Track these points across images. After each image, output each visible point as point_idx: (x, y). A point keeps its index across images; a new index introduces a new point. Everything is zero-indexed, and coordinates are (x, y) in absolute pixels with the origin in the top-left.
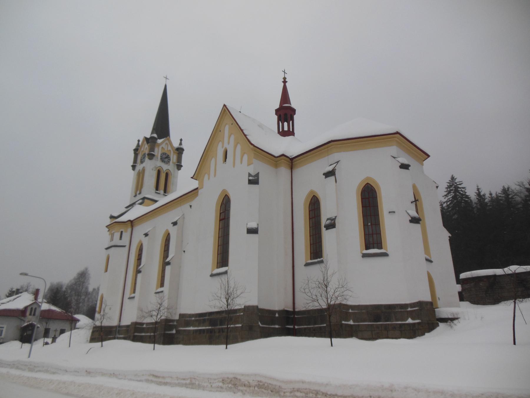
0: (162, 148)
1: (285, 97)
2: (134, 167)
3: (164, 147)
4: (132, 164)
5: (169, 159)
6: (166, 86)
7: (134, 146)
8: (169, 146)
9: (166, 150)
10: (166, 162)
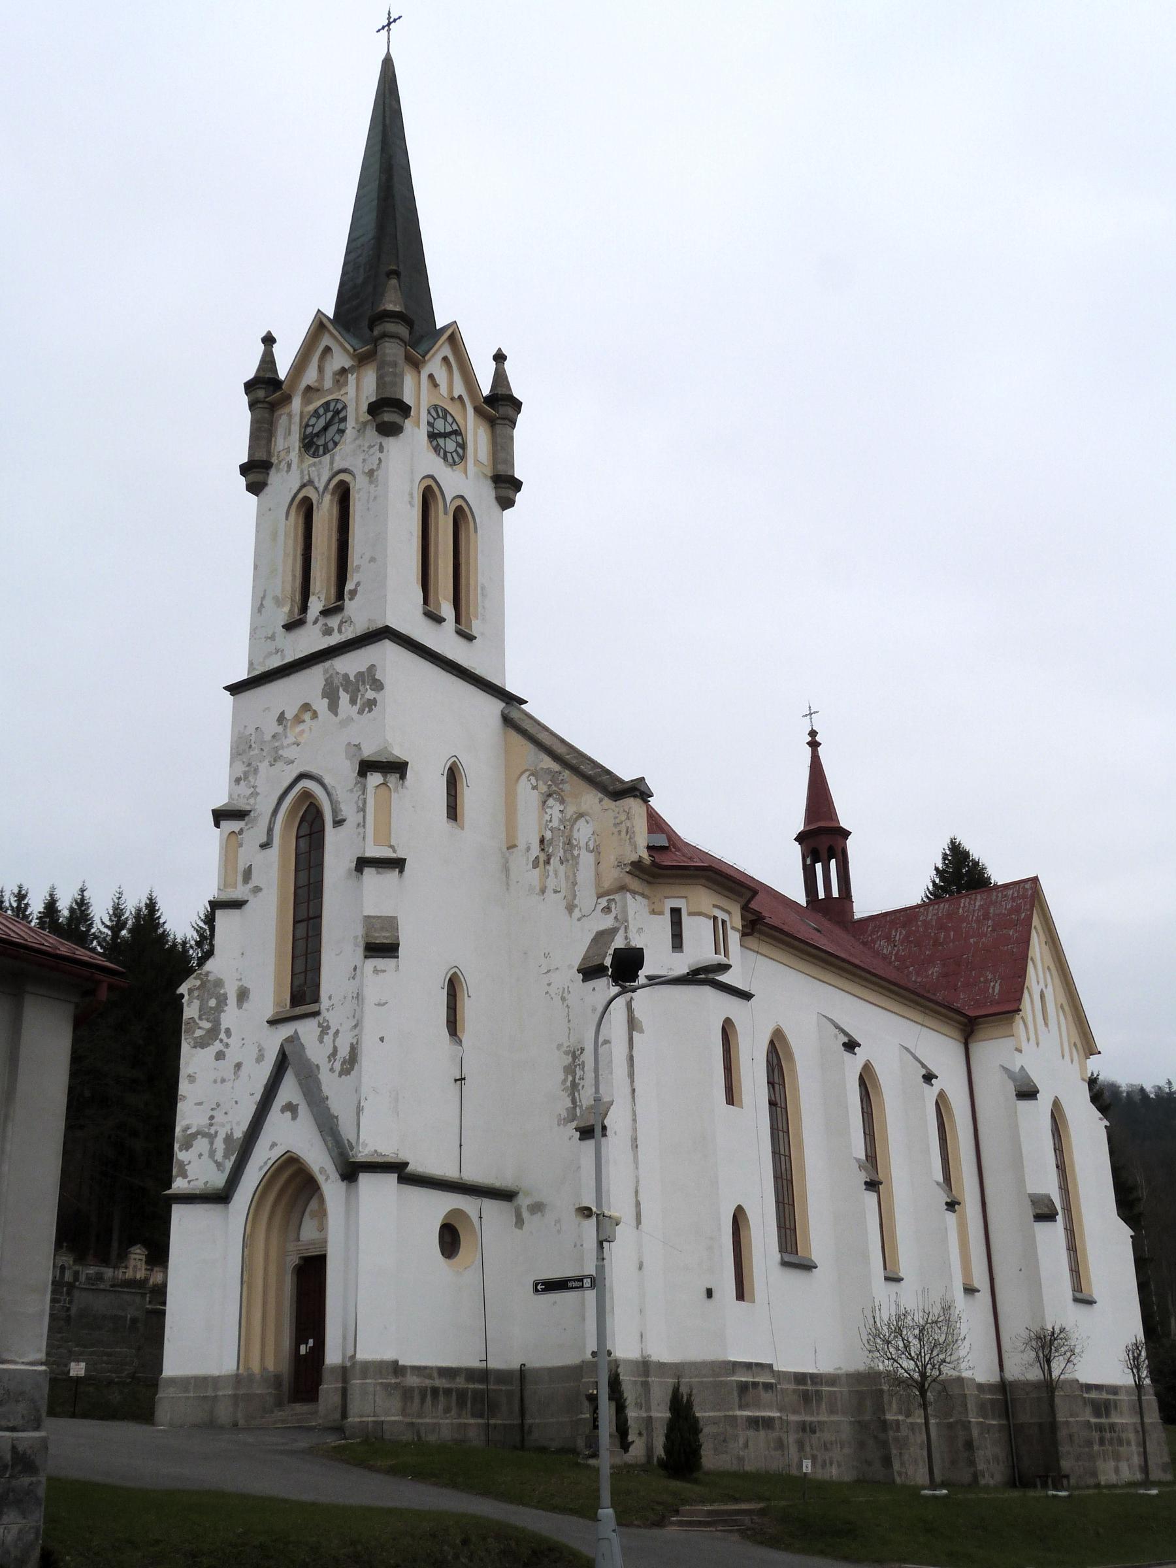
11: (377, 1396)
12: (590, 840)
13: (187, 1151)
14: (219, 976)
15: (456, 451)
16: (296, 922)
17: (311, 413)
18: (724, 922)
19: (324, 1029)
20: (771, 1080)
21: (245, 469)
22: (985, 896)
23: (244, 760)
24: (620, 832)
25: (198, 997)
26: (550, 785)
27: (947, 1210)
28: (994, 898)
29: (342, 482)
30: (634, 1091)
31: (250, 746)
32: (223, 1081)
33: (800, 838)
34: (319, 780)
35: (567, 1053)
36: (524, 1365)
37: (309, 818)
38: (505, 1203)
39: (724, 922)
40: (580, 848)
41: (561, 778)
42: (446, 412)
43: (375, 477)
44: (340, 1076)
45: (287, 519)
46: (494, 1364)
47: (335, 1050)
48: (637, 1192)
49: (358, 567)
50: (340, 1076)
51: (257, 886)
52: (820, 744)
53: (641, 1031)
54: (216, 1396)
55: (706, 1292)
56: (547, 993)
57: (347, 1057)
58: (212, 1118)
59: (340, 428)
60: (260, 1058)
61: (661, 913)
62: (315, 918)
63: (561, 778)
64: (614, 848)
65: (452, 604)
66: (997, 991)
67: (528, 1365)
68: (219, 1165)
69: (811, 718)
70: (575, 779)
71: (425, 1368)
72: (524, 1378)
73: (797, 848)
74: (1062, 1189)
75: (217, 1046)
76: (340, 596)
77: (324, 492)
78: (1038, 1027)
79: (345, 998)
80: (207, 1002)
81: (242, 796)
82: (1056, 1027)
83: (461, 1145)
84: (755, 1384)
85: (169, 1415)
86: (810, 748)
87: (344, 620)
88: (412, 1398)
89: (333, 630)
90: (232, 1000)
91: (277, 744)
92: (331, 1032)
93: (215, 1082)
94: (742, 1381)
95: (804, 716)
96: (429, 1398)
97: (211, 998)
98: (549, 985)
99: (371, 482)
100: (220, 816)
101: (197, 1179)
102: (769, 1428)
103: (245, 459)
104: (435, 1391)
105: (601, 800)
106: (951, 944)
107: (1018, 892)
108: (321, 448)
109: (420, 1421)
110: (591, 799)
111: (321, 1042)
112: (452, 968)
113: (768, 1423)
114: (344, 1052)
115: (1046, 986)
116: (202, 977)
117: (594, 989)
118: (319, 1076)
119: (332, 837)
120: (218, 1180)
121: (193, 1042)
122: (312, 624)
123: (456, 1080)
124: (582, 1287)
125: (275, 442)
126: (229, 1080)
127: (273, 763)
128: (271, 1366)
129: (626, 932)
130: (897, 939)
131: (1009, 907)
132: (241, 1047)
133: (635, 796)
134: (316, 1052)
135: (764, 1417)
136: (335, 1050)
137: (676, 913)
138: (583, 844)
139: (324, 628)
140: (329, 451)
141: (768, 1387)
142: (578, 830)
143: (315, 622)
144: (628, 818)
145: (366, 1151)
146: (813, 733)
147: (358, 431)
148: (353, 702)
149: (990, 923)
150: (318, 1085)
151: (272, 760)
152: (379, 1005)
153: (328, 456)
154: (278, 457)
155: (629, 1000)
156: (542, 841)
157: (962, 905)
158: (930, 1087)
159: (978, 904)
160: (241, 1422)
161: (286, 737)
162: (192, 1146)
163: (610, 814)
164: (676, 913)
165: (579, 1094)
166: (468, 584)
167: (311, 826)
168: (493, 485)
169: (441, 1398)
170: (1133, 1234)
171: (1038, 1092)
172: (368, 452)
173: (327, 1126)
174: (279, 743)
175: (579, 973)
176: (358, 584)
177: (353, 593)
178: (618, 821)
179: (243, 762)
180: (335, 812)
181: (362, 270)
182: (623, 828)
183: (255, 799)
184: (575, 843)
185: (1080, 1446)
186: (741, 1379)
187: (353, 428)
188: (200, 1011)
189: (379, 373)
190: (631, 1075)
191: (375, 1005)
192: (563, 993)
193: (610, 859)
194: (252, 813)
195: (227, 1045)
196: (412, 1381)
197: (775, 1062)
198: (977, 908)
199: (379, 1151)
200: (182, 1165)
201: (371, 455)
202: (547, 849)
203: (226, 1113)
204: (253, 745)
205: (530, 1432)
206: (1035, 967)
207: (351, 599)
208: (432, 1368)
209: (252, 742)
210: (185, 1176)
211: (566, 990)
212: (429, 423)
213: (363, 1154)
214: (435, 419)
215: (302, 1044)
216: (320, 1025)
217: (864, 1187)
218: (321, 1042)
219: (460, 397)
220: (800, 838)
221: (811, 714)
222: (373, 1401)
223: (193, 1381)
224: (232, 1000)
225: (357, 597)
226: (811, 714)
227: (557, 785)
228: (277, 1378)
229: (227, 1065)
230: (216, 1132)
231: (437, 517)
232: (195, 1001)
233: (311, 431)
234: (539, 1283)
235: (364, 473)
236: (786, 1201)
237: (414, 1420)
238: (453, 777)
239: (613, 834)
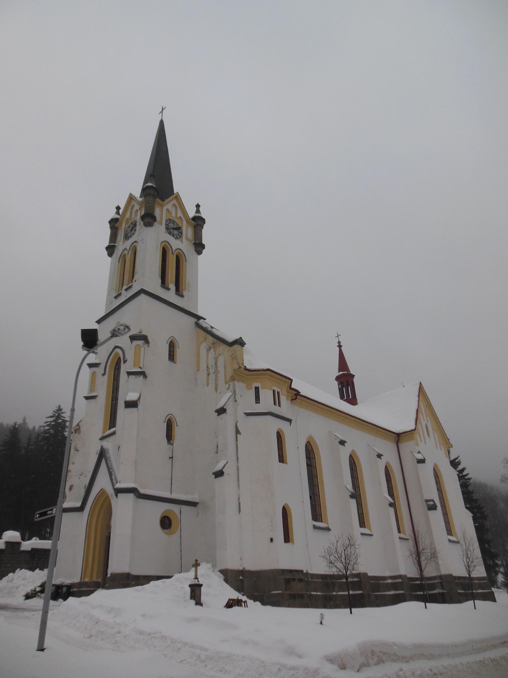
0: (168, 210)
1: (343, 364)
2: (110, 250)
3: (170, 210)
4: (107, 244)
5: (180, 231)
6: (162, 123)
7: (112, 214)
8: (179, 210)
9: (174, 214)
10: (175, 236)
15: (178, 234)
18: (278, 393)
27: (350, 498)
30: (238, 458)
39: (278, 393)
42: (174, 221)
45: (119, 262)
52: (342, 346)
53: (240, 434)
55: (270, 540)
61: (251, 389)
65: (175, 285)
69: (338, 338)
73: (336, 383)
74: (441, 498)
77: (129, 251)
83: (171, 484)
95: (336, 337)
115: (428, 422)
117: (221, 418)
119: (122, 366)
129: (235, 396)
137: (257, 389)
141: (300, 580)
146: (339, 342)
158: (381, 460)
164: (257, 389)
166: (182, 279)
170: (472, 515)
175: (216, 412)
180: (124, 358)
197: (353, 462)
206: (423, 415)
212: (166, 224)
214: (169, 223)
217: (349, 497)
221: (338, 336)
231: (169, 255)
238: (172, 346)
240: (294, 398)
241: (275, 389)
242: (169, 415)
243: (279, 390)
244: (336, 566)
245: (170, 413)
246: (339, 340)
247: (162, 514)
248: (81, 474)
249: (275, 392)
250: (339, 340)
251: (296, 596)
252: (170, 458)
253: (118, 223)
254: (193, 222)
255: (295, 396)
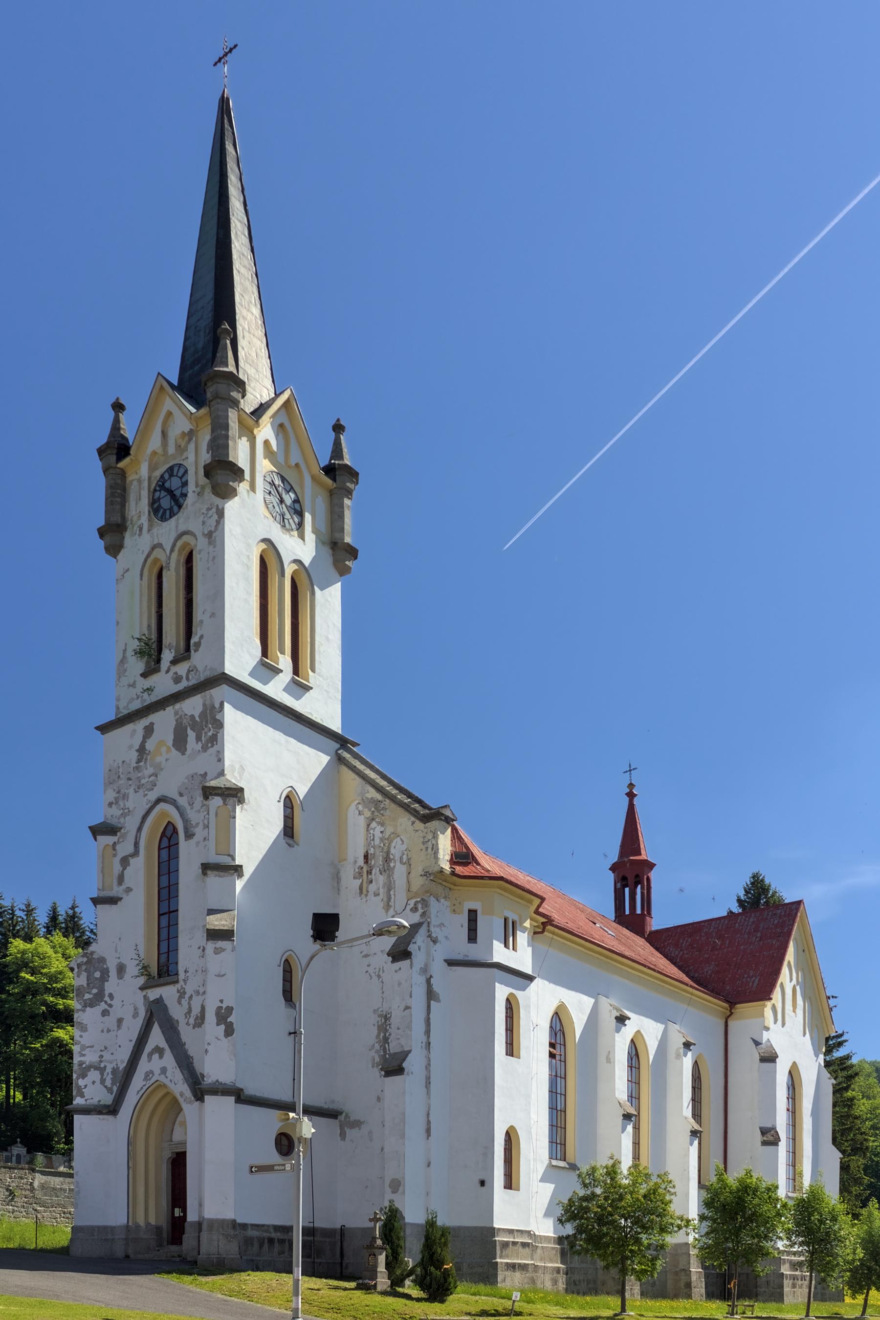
11: (220, 1242)
12: (404, 854)
13: (83, 1079)
14: (101, 955)
16: (160, 915)
17: (158, 479)
19: (182, 994)
20: (553, 1041)
21: (102, 533)
22: (758, 914)
23: (115, 788)
24: (427, 848)
25: (86, 970)
26: (374, 812)
28: (765, 916)
29: (186, 544)
30: (429, 1043)
31: (119, 777)
32: (109, 1031)
33: (613, 868)
34: (173, 802)
35: (380, 1016)
36: (344, 1226)
37: (168, 834)
38: (333, 1120)
40: (395, 862)
41: (382, 806)
43: (213, 538)
44: (194, 1028)
45: (141, 579)
46: (317, 1224)
47: (190, 1010)
48: (428, 1114)
49: (202, 622)
50: (194, 1028)
51: (128, 888)
53: (438, 1000)
54: (113, 1239)
56: (367, 972)
57: (199, 1015)
58: (101, 1056)
59: (183, 492)
60: (135, 1015)
62: (174, 911)
63: (382, 806)
64: (129, 779)
66: (755, 984)
67: (347, 1226)
68: (110, 1090)
69: (631, 774)
70: (393, 806)
71: (263, 1226)
72: (344, 1235)
73: (611, 876)
75: (103, 1006)
76: (188, 649)
78: (787, 1011)
79: (197, 971)
80: (94, 974)
81: (114, 816)
82: (802, 1012)
84: (514, 1243)
85: (80, 1250)
86: (628, 798)
87: (191, 669)
88: (252, 1244)
89: (182, 678)
90: (113, 973)
91: (139, 775)
92: (187, 996)
93: (102, 1031)
94: (504, 1241)
95: (625, 772)
96: (266, 1245)
97: (96, 971)
98: (369, 966)
99: (210, 543)
100: (97, 831)
101: (92, 1099)
102: (523, 1270)
103: (102, 522)
104: (271, 1241)
105: (413, 823)
106: (725, 950)
107: (785, 912)
108: (168, 512)
109: (257, 1258)
110: (405, 821)
111: (179, 1003)
112: (285, 952)
113: (523, 1267)
114: (196, 1010)
116: (88, 955)
118: (179, 1028)
119: (185, 847)
120: (108, 1099)
121: (83, 1003)
122: (165, 673)
123: (290, 1034)
124: (284, 1170)
125: (129, 508)
126: (114, 1030)
127: (137, 790)
128: (152, 1221)
130: (683, 945)
131: (776, 922)
132: (122, 1007)
133: (441, 819)
134: (176, 1012)
135: (520, 1263)
136: (190, 1010)
137: (473, 916)
138: (397, 858)
139: (175, 676)
140: (174, 515)
142: (395, 847)
143: (167, 672)
144: (434, 837)
145: (210, 1081)
146: (631, 786)
147: (198, 494)
148: (198, 739)
149: (759, 934)
150: (178, 1035)
151: (136, 787)
152: (219, 976)
153: (173, 519)
154: (132, 521)
155: (428, 977)
156: (366, 857)
157: (739, 921)
159: (752, 920)
160: (132, 1256)
161: (146, 769)
162: (87, 1076)
163: (420, 834)
164: (473, 916)
165: (389, 1046)
167: (169, 840)
168: (330, 551)
169: (276, 1244)
171: (777, 1057)
172: (206, 514)
173: (185, 1063)
174: (142, 774)
176: (202, 637)
177: (198, 645)
178: (426, 840)
179: (114, 790)
181: (202, 333)
182: (430, 845)
183: (125, 819)
184: (392, 857)
185: (773, 1288)
186: (503, 1239)
187: (194, 492)
188: (88, 980)
189: (213, 436)
190: (428, 1032)
191: (216, 975)
192: (379, 971)
193: (418, 870)
194: (123, 829)
195: (110, 1006)
196: (251, 1233)
197: (634, 1053)
198: (750, 923)
199: (220, 1080)
200: (79, 1088)
201: (210, 517)
202: (369, 862)
203: (112, 1054)
204: (121, 776)
205: (347, 1268)
207: (196, 651)
208: (268, 1226)
209: (120, 773)
210: (82, 1096)
211: (381, 969)
213: (209, 1080)
215: (165, 1005)
216: (178, 991)
218: (179, 1003)
219: (297, 465)
220: (613, 868)
221: (630, 770)
222: (217, 1246)
223: (96, 1229)
224: (113, 973)
225: (201, 649)
226: (630, 770)
227: (378, 811)
228: (158, 1229)
229: (111, 1021)
230: (105, 1067)
232: (83, 973)
233: (158, 495)
234: (253, 1167)
235: (204, 534)
236: (559, 1125)
237: (254, 1258)
239: (421, 850)
240: (541, 930)
241: (508, 916)
242: (287, 951)
243: (516, 918)
244: (683, 1254)
245: (289, 949)
246: (631, 780)
247: (279, 1130)
248: (103, 1049)
249: (509, 921)
250: (631, 780)
251: (517, 1267)
252: (290, 1034)
253: (127, 460)
254: (328, 481)
255: (542, 927)
